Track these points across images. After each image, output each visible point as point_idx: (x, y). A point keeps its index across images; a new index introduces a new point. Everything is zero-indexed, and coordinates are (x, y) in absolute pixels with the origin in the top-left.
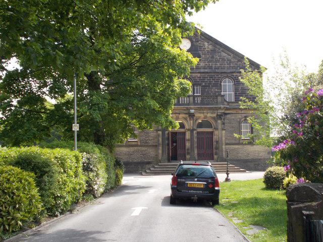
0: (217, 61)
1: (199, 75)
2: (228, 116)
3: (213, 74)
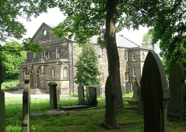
0: (54, 39)
1: (49, 46)
2: (48, 67)
3: (53, 45)
